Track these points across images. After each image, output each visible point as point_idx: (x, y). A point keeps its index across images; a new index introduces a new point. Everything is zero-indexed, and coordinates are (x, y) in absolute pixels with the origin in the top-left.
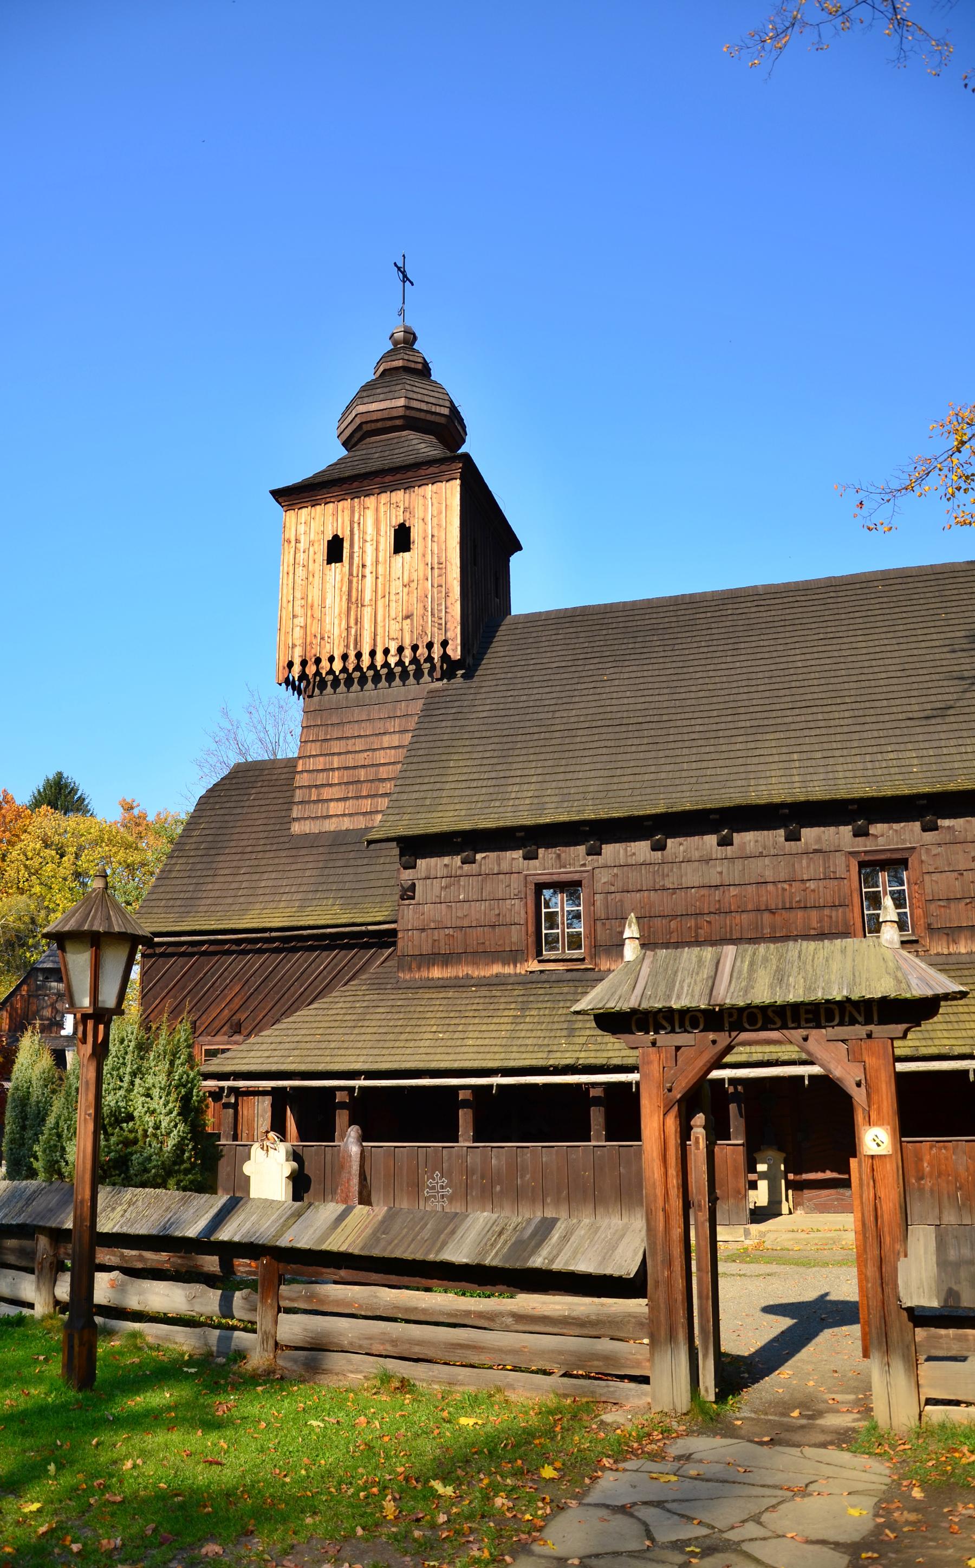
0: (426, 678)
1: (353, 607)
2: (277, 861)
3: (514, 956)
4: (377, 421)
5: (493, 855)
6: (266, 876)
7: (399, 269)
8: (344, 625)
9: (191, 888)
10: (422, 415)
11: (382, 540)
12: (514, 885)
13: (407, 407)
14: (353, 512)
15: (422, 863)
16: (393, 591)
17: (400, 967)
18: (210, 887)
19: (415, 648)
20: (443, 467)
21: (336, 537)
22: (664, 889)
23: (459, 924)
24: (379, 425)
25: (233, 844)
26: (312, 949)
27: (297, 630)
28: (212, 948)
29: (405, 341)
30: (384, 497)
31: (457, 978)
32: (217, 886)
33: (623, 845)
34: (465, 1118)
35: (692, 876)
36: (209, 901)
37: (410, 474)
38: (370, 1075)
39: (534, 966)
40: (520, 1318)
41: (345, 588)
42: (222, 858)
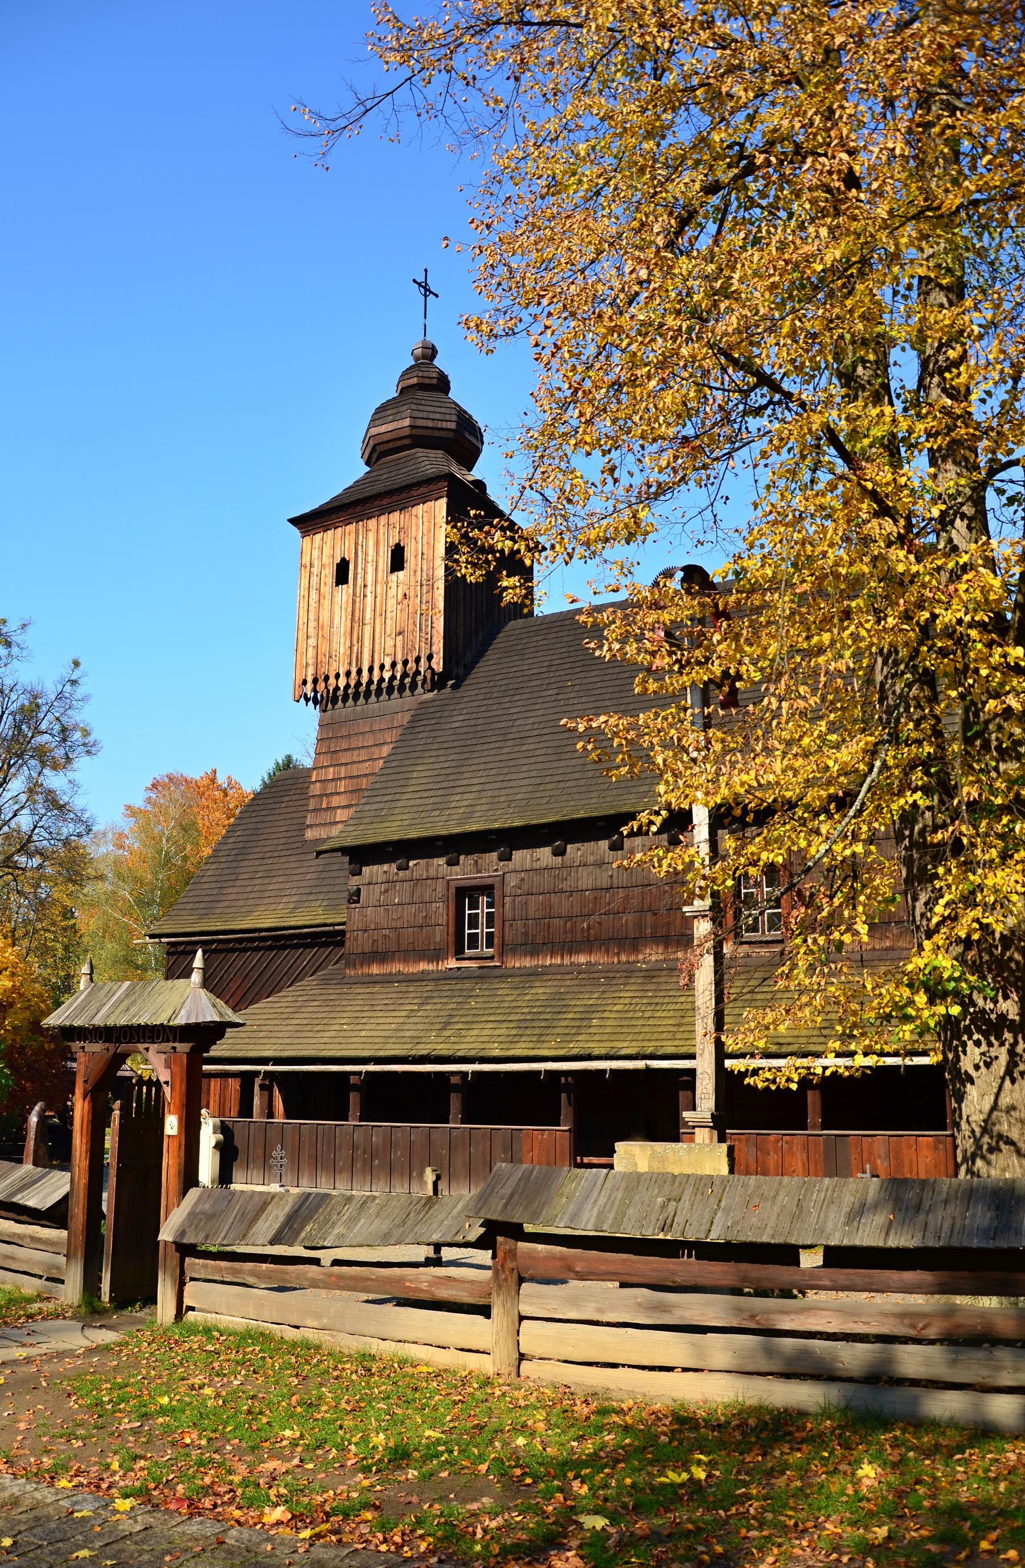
0: (420, 690)
1: (356, 626)
2: (287, 865)
3: (437, 956)
4: (388, 442)
5: (423, 862)
6: (275, 880)
7: (420, 284)
8: (348, 644)
9: (215, 892)
10: (429, 432)
11: (381, 560)
12: (439, 889)
13: (412, 427)
14: (357, 535)
15: (366, 870)
16: (389, 609)
17: (347, 965)
18: (230, 890)
19: (405, 663)
20: (432, 487)
21: (343, 559)
22: (562, 891)
23: (394, 925)
24: (391, 445)
25: (257, 850)
26: (297, 947)
27: (310, 649)
28: (220, 946)
29: (424, 357)
30: (383, 519)
31: (391, 974)
32: (235, 890)
33: (530, 851)
34: (455, 1102)
35: (586, 879)
36: (225, 904)
37: (404, 495)
38: (278, 1061)
39: (452, 963)
40: (34, 1239)
41: (350, 609)
42: (246, 863)
